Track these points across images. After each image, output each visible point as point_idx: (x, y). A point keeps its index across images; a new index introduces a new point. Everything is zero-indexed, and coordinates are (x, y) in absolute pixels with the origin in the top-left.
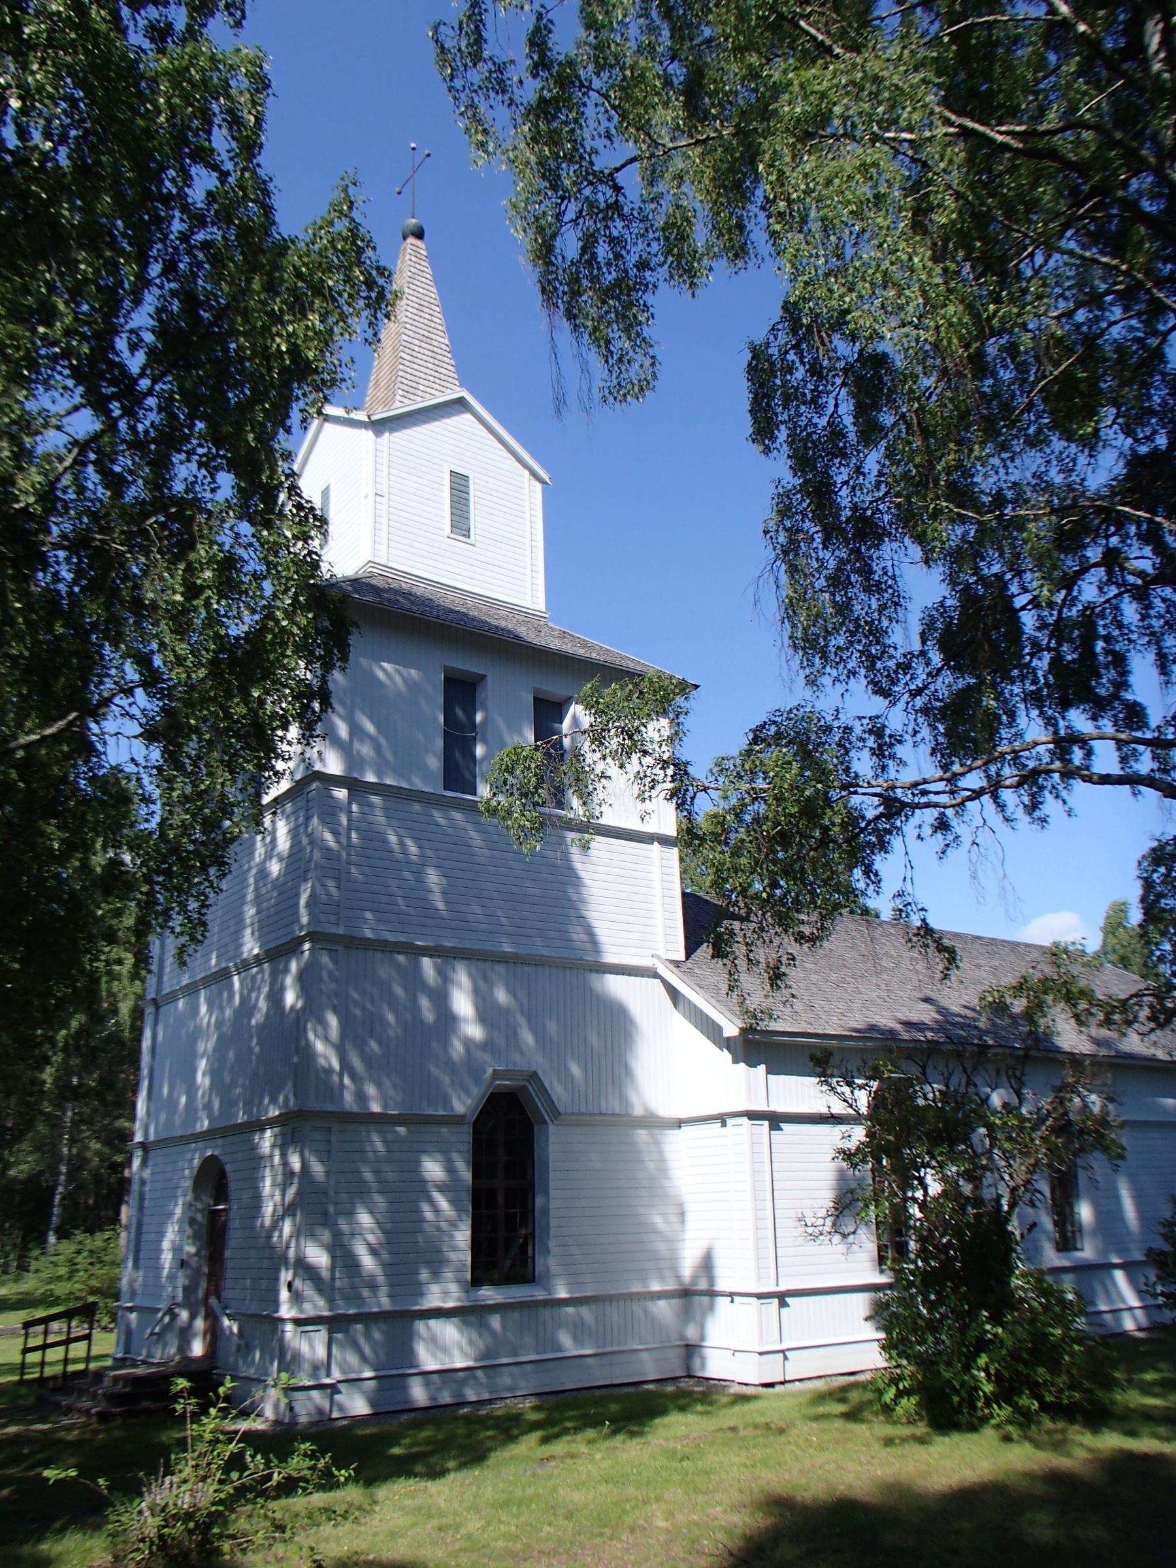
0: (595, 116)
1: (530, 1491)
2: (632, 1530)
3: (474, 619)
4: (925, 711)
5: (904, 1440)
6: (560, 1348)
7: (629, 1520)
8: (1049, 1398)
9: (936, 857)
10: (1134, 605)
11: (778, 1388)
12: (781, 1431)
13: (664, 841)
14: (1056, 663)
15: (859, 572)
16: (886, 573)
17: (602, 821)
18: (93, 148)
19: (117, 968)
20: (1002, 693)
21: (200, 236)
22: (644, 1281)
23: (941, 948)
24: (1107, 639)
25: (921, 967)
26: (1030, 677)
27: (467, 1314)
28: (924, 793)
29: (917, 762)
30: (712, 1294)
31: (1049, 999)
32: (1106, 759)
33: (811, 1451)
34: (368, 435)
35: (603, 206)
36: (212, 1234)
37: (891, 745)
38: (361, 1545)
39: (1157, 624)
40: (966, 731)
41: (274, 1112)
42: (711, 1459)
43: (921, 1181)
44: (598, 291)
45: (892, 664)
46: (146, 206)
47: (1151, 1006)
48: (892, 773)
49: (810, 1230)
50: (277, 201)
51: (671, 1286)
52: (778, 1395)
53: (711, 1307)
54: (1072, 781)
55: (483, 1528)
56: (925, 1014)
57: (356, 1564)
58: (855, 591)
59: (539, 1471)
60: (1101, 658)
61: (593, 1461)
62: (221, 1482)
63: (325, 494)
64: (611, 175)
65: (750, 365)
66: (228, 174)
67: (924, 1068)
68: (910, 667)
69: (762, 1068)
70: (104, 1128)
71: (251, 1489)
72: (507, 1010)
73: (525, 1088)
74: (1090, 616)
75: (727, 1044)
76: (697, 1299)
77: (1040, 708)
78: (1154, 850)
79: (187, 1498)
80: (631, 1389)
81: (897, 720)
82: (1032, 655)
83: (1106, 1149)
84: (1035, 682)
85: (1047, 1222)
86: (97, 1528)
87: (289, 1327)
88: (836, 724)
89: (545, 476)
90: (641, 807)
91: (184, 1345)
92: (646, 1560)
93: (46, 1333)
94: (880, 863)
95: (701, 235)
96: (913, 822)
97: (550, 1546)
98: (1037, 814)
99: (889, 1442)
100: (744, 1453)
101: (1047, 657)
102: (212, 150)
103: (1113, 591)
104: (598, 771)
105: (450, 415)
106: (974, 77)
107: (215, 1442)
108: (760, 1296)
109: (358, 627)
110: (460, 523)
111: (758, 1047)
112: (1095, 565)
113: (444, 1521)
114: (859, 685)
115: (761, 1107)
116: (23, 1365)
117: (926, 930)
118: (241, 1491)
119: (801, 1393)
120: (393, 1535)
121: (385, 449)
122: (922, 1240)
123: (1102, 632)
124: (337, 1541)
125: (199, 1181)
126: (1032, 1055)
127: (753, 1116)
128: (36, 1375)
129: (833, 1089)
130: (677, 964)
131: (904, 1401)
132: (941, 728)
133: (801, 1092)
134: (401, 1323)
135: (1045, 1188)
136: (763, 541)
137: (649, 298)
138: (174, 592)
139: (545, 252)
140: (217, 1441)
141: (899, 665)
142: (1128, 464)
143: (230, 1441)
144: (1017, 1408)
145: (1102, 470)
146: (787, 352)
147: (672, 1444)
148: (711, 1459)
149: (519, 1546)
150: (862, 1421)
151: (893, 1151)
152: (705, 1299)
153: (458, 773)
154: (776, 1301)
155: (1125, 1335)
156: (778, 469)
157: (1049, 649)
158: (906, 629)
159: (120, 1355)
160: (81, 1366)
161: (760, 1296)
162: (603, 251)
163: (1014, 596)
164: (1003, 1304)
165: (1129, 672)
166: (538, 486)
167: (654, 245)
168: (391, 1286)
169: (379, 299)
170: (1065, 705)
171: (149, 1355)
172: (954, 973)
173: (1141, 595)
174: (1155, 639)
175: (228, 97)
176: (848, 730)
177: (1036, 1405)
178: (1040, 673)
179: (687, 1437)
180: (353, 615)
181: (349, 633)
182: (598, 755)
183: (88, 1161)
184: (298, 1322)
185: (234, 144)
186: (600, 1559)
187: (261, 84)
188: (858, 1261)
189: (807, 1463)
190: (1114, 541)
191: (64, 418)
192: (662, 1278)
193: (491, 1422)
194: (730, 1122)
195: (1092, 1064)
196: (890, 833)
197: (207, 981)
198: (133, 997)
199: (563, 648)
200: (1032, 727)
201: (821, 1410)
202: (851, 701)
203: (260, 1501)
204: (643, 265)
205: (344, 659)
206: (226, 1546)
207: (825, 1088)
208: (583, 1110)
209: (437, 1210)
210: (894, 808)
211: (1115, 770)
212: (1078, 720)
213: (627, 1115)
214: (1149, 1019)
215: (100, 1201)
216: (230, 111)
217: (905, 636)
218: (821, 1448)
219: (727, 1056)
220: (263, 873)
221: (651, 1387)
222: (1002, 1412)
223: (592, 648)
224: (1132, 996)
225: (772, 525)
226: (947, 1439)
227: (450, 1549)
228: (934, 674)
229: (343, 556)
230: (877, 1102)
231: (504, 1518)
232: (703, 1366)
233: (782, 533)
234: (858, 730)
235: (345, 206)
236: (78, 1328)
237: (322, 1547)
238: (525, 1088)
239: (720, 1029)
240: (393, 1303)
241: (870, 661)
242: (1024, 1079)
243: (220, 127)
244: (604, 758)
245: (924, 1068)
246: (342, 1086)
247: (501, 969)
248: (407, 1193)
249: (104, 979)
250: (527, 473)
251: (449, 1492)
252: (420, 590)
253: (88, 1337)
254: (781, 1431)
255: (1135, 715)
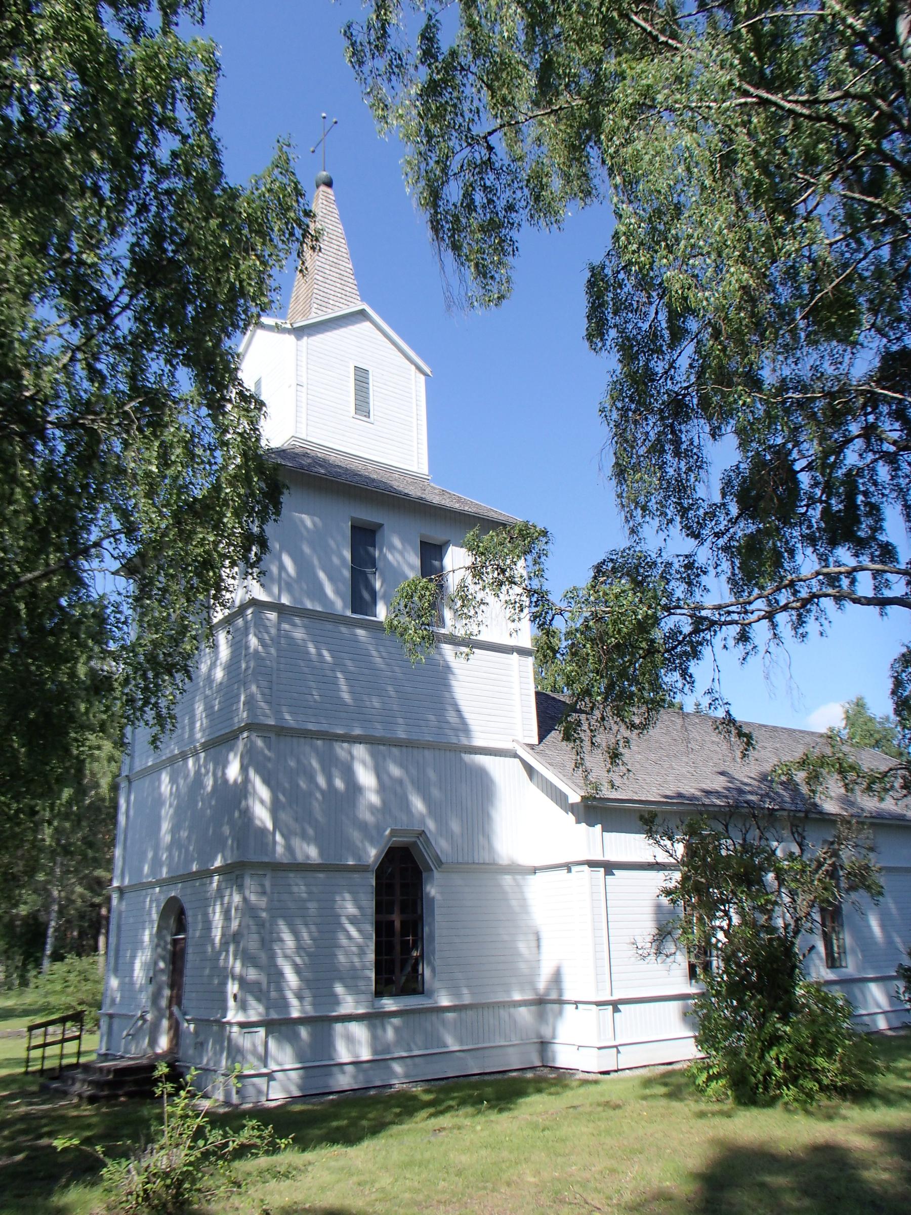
0: (473, 92)
1: (427, 1155)
2: (508, 1184)
3: (373, 480)
4: (726, 549)
5: (714, 1114)
6: (446, 1046)
7: (505, 1177)
8: (826, 1082)
9: (738, 662)
10: (887, 468)
11: (613, 1075)
12: (617, 1107)
13: (522, 652)
14: (827, 513)
15: (671, 442)
16: (692, 444)
17: (479, 638)
18: (83, 119)
19: (97, 752)
20: (784, 535)
21: (165, 185)
22: (508, 992)
23: (740, 734)
24: (866, 494)
25: (725, 746)
26: (806, 523)
27: (374, 1019)
28: (729, 613)
29: (716, 591)
30: (561, 1002)
31: (824, 771)
32: (865, 585)
33: (644, 1123)
34: (291, 338)
35: (479, 162)
36: (176, 958)
37: (698, 575)
38: (299, 1197)
39: (903, 482)
40: (757, 563)
41: (218, 863)
42: (565, 1130)
43: (726, 913)
44: (472, 226)
45: (701, 512)
46: (126, 163)
47: (904, 777)
48: (698, 598)
49: (640, 952)
50: (224, 158)
51: (529, 996)
52: (613, 1081)
53: (560, 1013)
54: (843, 602)
55: (393, 1184)
56: (719, 783)
57: (296, 1211)
58: (669, 457)
59: (433, 1139)
60: (862, 508)
61: (474, 1131)
62: (190, 1148)
63: (258, 384)
64: (485, 138)
65: (589, 281)
66: (189, 136)
67: (726, 826)
68: (715, 516)
69: (599, 827)
70: (86, 876)
71: (214, 1153)
72: (400, 782)
73: (415, 843)
74: (851, 478)
75: (572, 809)
76: (549, 1006)
77: (814, 546)
78: (903, 655)
79: (165, 1161)
80: (499, 1076)
81: (704, 555)
82: (808, 506)
83: (868, 888)
84: (810, 527)
85: (821, 948)
86: (93, 1184)
87: (235, 1029)
88: (659, 560)
89: (428, 370)
90: (512, 626)
91: (153, 1042)
92: (521, 1207)
93: (46, 1034)
94: (694, 667)
95: (556, 183)
96: (720, 635)
97: (446, 1196)
98: (801, 631)
99: (702, 1115)
100: (591, 1125)
101: (819, 507)
102: (175, 119)
103: (870, 456)
104: (478, 599)
105: (353, 323)
106: (766, 62)
107: (185, 1117)
108: (598, 1004)
109: (288, 488)
110: (362, 407)
111: (596, 811)
112: (858, 436)
113: (362, 1178)
114: (676, 530)
115: (598, 857)
116: (28, 1060)
117: (730, 720)
118: (206, 1155)
119: (632, 1079)
120: (323, 1189)
121: (304, 349)
122: (727, 960)
123: (862, 488)
124: (281, 1194)
125: (164, 915)
126: (805, 818)
127: (592, 864)
128: (39, 1067)
129: (658, 842)
130: (532, 747)
131: (713, 1084)
132: (737, 562)
133: (633, 846)
134: (323, 1023)
135: (817, 917)
136: (598, 419)
137: (514, 234)
138: (150, 463)
139: (435, 195)
140: (187, 1116)
141: (706, 513)
142: (883, 358)
143: (197, 1116)
144: (801, 1089)
145: (863, 363)
146: (618, 272)
147: (535, 1118)
148: (565, 1130)
149: (421, 1197)
150: (681, 1100)
151: (699, 889)
152: (556, 1006)
153: (361, 599)
154: (610, 1007)
155: (878, 1032)
156: (608, 364)
157: (821, 502)
158: (708, 487)
159: (103, 1051)
160: (74, 1060)
161: (598, 1004)
162: (479, 198)
163: (795, 460)
164: (788, 1009)
165: (883, 519)
166: (422, 378)
167: (519, 192)
168: (314, 997)
169: (301, 231)
170: (833, 543)
171: (127, 1051)
172: (751, 753)
173: (891, 459)
174: (901, 492)
175: (189, 78)
176: (669, 565)
177: (816, 1087)
178: (814, 520)
179: (546, 1112)
180: (278, 479)
181: (282, 493)
182: (479, 587)
183: (73, 902)
184: (242, 1025)
185: (193, 114)
186: (485, 1206)
187: (214, 67)
188: (673, 976)
189: (641, 1132)
190: (871, 418)
191: (49, 324)
192: (522, 990)
193: (393, 1102)
194: (574, 869)
195: (858, 822)
196: (701, 644)
197: (172, 760)
198: (110, 775)
199: (443, 502)
200: (806, 562)
201: (648, 1092)
202: (667, 543)
203: (220, 1162)
204: (510, 208)
205: (278, 513)
206: (195, 1197)
207: (651, 841)
208: (460, 860)
209: (350, 937)
210: (701, 624)
211: (870, 594)
212: (844, 555)
213: (494, 864)
214: (902, 788)
215: (87, 930)
216: (190, 89)
217: (709, 489)
218: (651, 1121)
219: (571, 818)
220: (209, 679)
221: (514, 1074)
222: (789, 1093)
223: (465, 503)
224: (891, 769)
225: (608, 405)
226: (748, 1114)
227: (368, 1199)
228: (734, 522)
229: (275, 433)
230: (691, 852)
231: (408, 1176)
232: (554, 1060)
233: (615, 412)
234: (676, 566)
235: (283, 165)
236: (72, 1030)
237: (268, 1199)
238: (415, 843)
239: (566, 797)
240: (315, 1010)
241: (684, 512)
242: (805, 834)
243: (181, 100)
244: (484, 588)
245: (726, 826)
246: (274, 842)
247: (395, 751)
248: (329, 925)
249: (88, 761)
250: (413, 367)
251: (361, 1155)
252: (333, 458)
253: (78, 1038)
254: (617, 1107)
255: (888, 552)
